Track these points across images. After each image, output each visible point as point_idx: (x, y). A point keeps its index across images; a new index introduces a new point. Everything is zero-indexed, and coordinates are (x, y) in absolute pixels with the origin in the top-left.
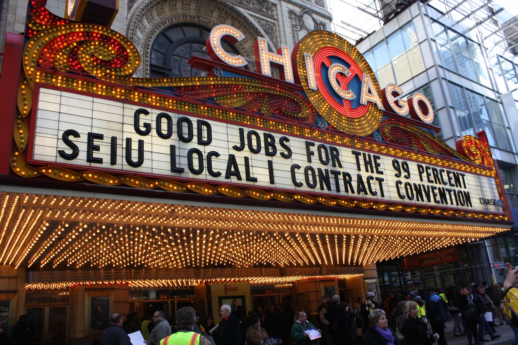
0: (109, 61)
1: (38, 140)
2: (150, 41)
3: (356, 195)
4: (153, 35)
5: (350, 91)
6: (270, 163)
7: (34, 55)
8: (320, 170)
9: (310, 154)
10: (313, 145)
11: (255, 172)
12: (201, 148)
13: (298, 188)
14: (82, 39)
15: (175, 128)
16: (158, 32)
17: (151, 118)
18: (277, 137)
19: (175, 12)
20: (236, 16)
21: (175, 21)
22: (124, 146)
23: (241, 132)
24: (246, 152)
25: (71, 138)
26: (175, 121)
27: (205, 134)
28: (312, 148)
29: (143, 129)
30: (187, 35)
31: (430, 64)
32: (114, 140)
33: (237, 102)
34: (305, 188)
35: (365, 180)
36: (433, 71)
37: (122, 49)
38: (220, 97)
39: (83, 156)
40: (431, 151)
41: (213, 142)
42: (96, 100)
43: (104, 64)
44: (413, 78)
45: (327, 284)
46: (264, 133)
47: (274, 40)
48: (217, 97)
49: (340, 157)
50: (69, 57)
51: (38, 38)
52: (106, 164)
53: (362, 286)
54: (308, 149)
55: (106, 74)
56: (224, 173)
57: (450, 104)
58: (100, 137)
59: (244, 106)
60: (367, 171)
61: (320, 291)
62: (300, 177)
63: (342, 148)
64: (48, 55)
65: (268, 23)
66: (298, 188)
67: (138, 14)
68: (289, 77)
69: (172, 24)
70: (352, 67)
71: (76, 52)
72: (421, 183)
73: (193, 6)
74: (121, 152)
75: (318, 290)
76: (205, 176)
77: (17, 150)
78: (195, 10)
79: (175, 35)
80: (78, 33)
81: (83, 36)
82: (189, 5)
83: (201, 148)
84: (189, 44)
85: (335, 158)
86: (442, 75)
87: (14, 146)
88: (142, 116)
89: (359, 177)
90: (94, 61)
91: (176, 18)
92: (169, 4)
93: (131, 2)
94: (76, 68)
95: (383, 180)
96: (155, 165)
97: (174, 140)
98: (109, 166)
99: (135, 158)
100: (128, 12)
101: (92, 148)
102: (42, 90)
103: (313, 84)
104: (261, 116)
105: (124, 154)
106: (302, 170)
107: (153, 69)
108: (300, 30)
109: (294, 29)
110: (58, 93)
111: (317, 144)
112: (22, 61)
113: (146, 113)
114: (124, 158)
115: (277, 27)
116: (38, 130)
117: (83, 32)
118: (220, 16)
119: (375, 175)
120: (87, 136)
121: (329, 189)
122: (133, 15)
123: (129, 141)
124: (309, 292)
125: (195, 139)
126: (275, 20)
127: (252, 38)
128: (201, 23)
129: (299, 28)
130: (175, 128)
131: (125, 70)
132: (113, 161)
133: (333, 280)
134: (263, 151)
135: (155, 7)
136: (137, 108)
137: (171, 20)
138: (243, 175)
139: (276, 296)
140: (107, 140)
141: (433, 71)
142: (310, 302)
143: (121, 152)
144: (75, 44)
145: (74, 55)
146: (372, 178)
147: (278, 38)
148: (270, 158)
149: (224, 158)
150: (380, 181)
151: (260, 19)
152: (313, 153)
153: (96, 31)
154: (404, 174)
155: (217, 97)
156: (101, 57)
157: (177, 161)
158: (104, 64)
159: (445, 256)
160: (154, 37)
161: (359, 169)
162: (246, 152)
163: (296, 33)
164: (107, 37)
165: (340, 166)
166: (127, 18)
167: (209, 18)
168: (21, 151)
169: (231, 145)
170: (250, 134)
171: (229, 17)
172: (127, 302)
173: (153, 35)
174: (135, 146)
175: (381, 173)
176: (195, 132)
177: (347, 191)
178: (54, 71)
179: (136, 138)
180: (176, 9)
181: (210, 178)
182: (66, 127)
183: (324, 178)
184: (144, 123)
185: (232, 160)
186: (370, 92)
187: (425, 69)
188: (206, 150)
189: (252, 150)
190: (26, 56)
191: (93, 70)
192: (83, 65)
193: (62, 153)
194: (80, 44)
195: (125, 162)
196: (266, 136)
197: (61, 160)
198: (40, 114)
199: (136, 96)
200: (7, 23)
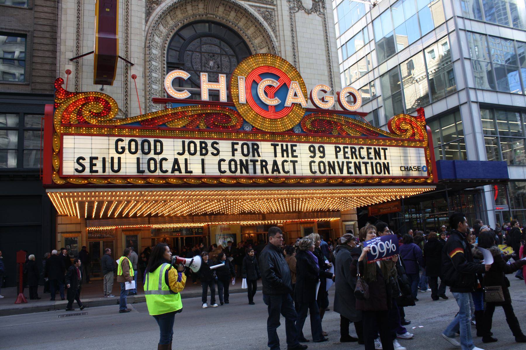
0: (100, 113)
1: (65, 164)
2: (166, 44)
3: (270, 174)
4: (168, 37)
5: (276, 98)
6: (203, 160)
7: (59, 118)
8: (241, 161)
9: (234, 150)
10: (237, 144)
11: (190, 168)
12: (156, 157)
13: (222, 174)
14: (84, 102)
15: (139, 147)
16: (172, 34)
17: (125, 143)
18: (209, 142)
19: (186, 13)
20: (238, 9)
21: (186, 22)
22: (110, 162)
23: (184, 143)
24: (186, 155)
25: (81, 161)
26: (139, 143)
27: (159, 148)
28: (236, 147)
29: (120, 150)
30: (198, 32)
31: (449, 15)
32: (104, 159)
33: (180, 124)
34: (228, 173)
35: (279, 163)
36: (451, 23)
37: (107, 103)
38: (170, 122)
39: (88, 170)
40: (352, 133)
41: (164, 152)
42: (93, 137)
43: (97, 115)
44: (435, 29)
45: (306, 225)
46: (200, 141)
47: (273, 25)
48: (168, 123)
49: (260, 150)
50: (77, 115)
51: (60, 107)
52: (100, 172)
53: (340, 227)
54: (233, 147)
55: (98, 121)
56: (170, 170)
57: (466, 55)
58: (96, 158)
59: (187, 125)
60: (283, 156)
61: (300, 231)
62: (225, 167)
63: (262, 143)
64: (66, 116)
65: (268, 10)
66: (222, 174)
67: (153, 25)
68: (223, 98)
69: (184, 24)
70: (282, 78)
71: (81, 111)
72: (336, 160)
73: (201, 6)
74: (108, 165)
75: (299, 230)
76: (158, 173)
77: (55, 171)
78: (203, 8)
79: (187, 34)
80: (81, 99)
81: (85, 100)
82: (198, 6)
83: (156, 157)
84: (199, 39)
85: (256, 150)
86: (461, 26)
87: (53, 169)
88: (120, 143)
89: (275, 163)
90: (91, 115)
91: (187, 20)
92: (180, 8)
93: (147, 16)
94: (82, 120)
95: (296, 162)
96: (128, 170)
97: (139, 154)
98: (102, 174)
99: (116, 167)
100: (146, 25)
101: (92, 165)
102: (65, 137)
103: (242, 99)
104: (200, 131)
105: (110, 166)
106: (227, 162)
107: (169, 65)
108: (297, 12)
109: (292, 11)
110: (72, 137)
111: (241, 143)
112: (53, 121)
113: (122, 141)
114: (110, 168)
115: (276, 12)
116: (64, 159)
117: (84, 98)
118: (225, 10)
119: (290, 158)
120: (89, 159)
121: (247, 172)
122: (150, 27)
123: (112, 159)
124: (291, 231)
125: (152, 152)
126: (274, 5)
127: (253, 25)
128: (209, 19)
129: (297, 9)
130: (139, 147)
131: (109, 116)
132: (104, 171)
133: (313, 222)
134: (198, 153)
135: (168, 14)
136: (116, 138)
137: (182, 22)
138: (183, 170)
139: (263, 234)
140: (100, 159)
141: (451, 23)
142: (292, 238)
143: (108, 165)
144: (80, 106)
145: (80, 113)
146: (287, 161)
147: (277, 22)
148: (203, 157)
149: (171, 161)
150: (294, 162)
151: (260, 7)
152: (236, 150)
153: (91, 95)
154: (318, 154)
155: (168, 123)
156: (95, 111)
157: (141, 165)
158: (97, 115)
159: (393, 207)
160: (169, 40)
161: (276, 156)
162: (186, 155)
163: (293, 15)
164: (98, 98)
165: (259, 156)
166: (145, 31)
167: (216, 13)
168: (57, 171)
169: (177, 152)
170: (189, 143)
171: (233, 10)
172: (150, 238)
173: (168, 37)
174: (116, 161)
175: (296, 157)
176: (152, 147)
177: (262, 172)
178: (70, 125)
179: (116, 156)
180: (187, 11)
181: (161, 174)
182: (77, 156)
183: (244, 166)
184: (121, 147)
185: (176, 161)
186: (295, 95)
187: (445, 21)
188: (158, 158)
189: (190, 154)
190: (55, 119)
191: (90, 120)
192: (85, 118)
193: (77, 170)
194: (83, 105)
195: (110, 171)
196: (201, 143)
197: (77, 174)
198: (64, 151)
199: (116, 131)
200: (61, 53)
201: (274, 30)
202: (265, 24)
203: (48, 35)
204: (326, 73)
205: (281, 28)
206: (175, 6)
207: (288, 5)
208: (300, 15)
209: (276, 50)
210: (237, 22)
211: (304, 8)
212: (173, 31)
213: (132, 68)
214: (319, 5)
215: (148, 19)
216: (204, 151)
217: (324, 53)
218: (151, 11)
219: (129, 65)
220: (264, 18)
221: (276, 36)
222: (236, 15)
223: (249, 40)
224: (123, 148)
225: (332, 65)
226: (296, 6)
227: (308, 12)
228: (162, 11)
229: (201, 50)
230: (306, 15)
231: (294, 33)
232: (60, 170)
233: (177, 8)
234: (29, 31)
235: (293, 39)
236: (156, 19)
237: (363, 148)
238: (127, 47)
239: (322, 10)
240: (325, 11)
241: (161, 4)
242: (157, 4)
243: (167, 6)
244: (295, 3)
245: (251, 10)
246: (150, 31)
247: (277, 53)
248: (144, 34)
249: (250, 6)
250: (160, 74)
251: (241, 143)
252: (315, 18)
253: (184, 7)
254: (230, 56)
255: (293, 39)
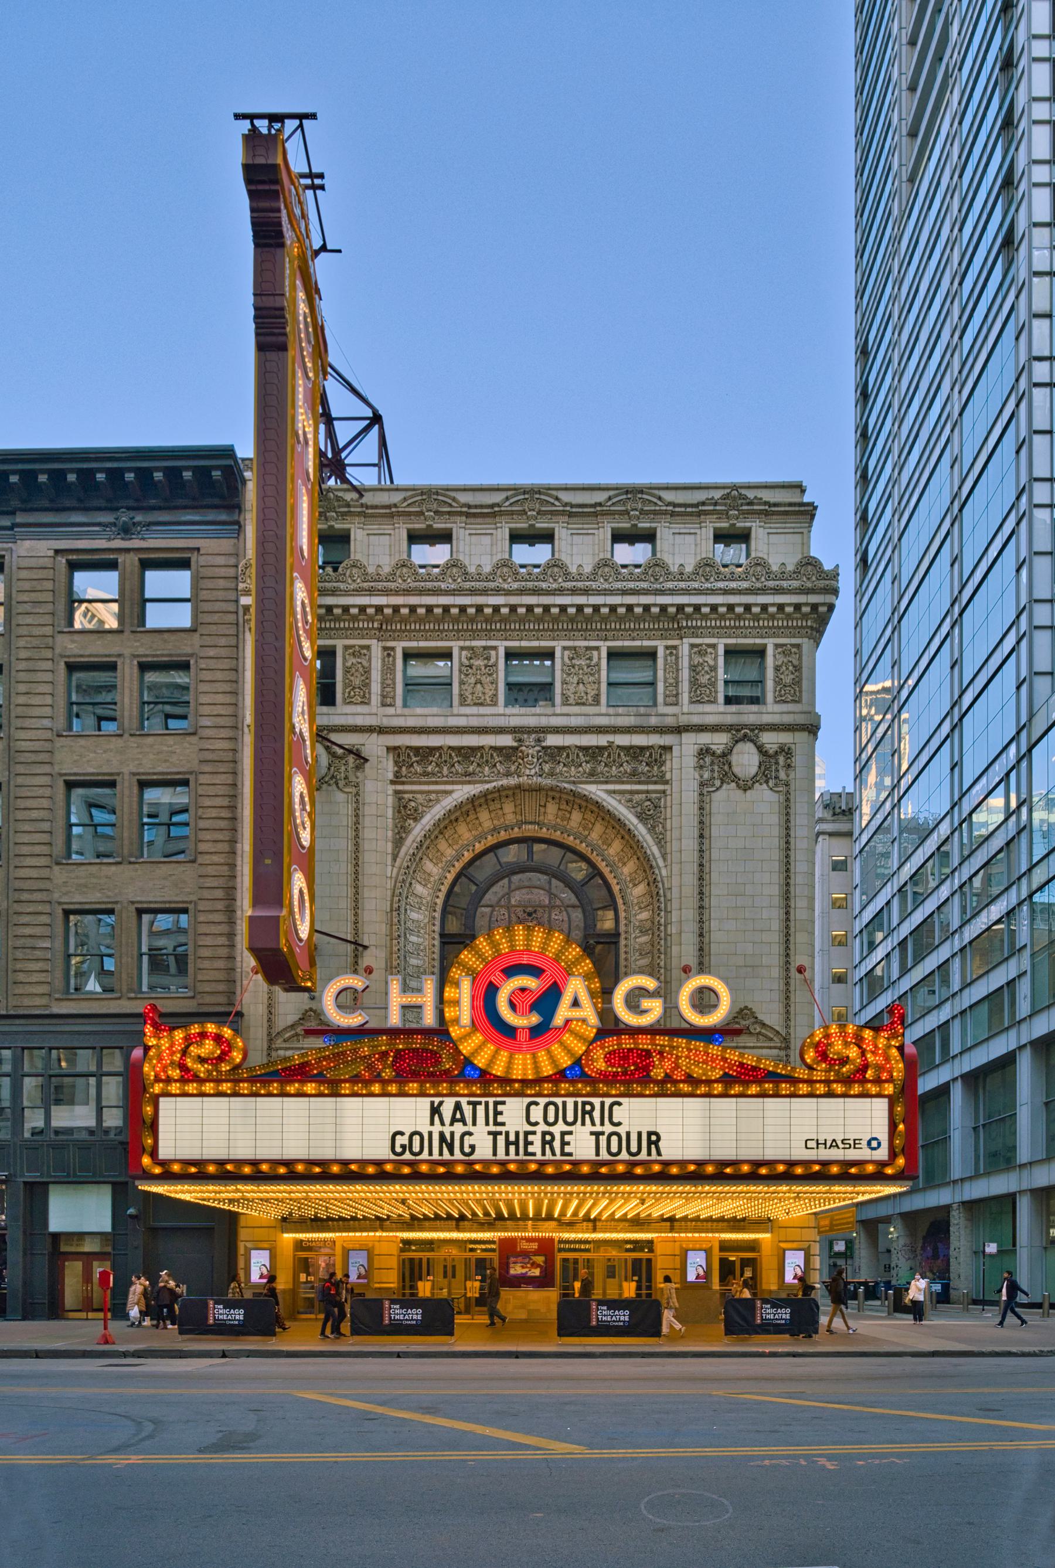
100: (393, 866)
115: (669, 798)
121: (452, 1153)
126: (666, 782)
129: (718, 783)
171: (575, 806)
175: (503, 1124)
186: (576, 1003)
201: (661, 842)
202: (641, 830)
203: (220, 905)
204: (776, 925)
205: (676, 834)
206: (453, 818)
207: (697, 776)
208: (725, 797)
209: (660, 885)
210: (587, 833)
211: (736, 779)
212: (452, 869)
213: (367, 953)
214: (777, 763)
215: (399, 852)
216: (654, 1138)
217: (777, 878)
218: (404, 835)
219: (360, 949)
220: (640, 816)
221: (664, 856)
222: (584, 819)
223: (609, 869)
224: (403, 1146)
225: (793, 906)
226: (716, 775)
227: (745, 786)
228: (423, 833)
229: (509, 901)
230: (740, 792)
231: (706, 841)
232: (154, 1153)
233: (457, 820)
234: (191, 902)
235: (702, 857)
236: (411, 851)
237: (537, 1104)
238: (356, 915)
239: (782, 775)
240: (792, 776)
241: (421, 818)
242: (415, 820)
243: (432, 822)
244: (716, 768)
245: (612, 803)
246: (400, 878)
247: (661, 892)
248: (389, 884)
249: (610, 792)
250: (426, 959)
251: (542, 1101)
252: (765, 796)
253: (472, 816)
254: (569, 909)
255: (702, 857)
